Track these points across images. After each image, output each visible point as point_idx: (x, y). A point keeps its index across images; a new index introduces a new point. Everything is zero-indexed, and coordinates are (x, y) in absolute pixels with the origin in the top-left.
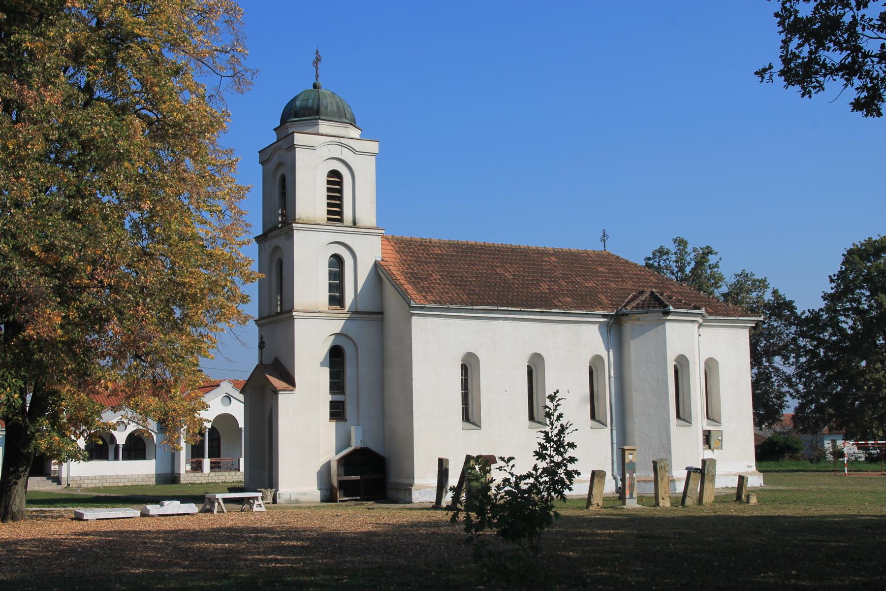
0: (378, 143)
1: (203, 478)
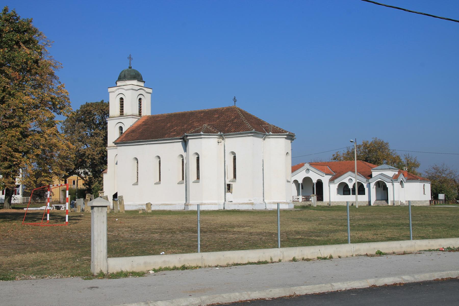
0: (152, 90)
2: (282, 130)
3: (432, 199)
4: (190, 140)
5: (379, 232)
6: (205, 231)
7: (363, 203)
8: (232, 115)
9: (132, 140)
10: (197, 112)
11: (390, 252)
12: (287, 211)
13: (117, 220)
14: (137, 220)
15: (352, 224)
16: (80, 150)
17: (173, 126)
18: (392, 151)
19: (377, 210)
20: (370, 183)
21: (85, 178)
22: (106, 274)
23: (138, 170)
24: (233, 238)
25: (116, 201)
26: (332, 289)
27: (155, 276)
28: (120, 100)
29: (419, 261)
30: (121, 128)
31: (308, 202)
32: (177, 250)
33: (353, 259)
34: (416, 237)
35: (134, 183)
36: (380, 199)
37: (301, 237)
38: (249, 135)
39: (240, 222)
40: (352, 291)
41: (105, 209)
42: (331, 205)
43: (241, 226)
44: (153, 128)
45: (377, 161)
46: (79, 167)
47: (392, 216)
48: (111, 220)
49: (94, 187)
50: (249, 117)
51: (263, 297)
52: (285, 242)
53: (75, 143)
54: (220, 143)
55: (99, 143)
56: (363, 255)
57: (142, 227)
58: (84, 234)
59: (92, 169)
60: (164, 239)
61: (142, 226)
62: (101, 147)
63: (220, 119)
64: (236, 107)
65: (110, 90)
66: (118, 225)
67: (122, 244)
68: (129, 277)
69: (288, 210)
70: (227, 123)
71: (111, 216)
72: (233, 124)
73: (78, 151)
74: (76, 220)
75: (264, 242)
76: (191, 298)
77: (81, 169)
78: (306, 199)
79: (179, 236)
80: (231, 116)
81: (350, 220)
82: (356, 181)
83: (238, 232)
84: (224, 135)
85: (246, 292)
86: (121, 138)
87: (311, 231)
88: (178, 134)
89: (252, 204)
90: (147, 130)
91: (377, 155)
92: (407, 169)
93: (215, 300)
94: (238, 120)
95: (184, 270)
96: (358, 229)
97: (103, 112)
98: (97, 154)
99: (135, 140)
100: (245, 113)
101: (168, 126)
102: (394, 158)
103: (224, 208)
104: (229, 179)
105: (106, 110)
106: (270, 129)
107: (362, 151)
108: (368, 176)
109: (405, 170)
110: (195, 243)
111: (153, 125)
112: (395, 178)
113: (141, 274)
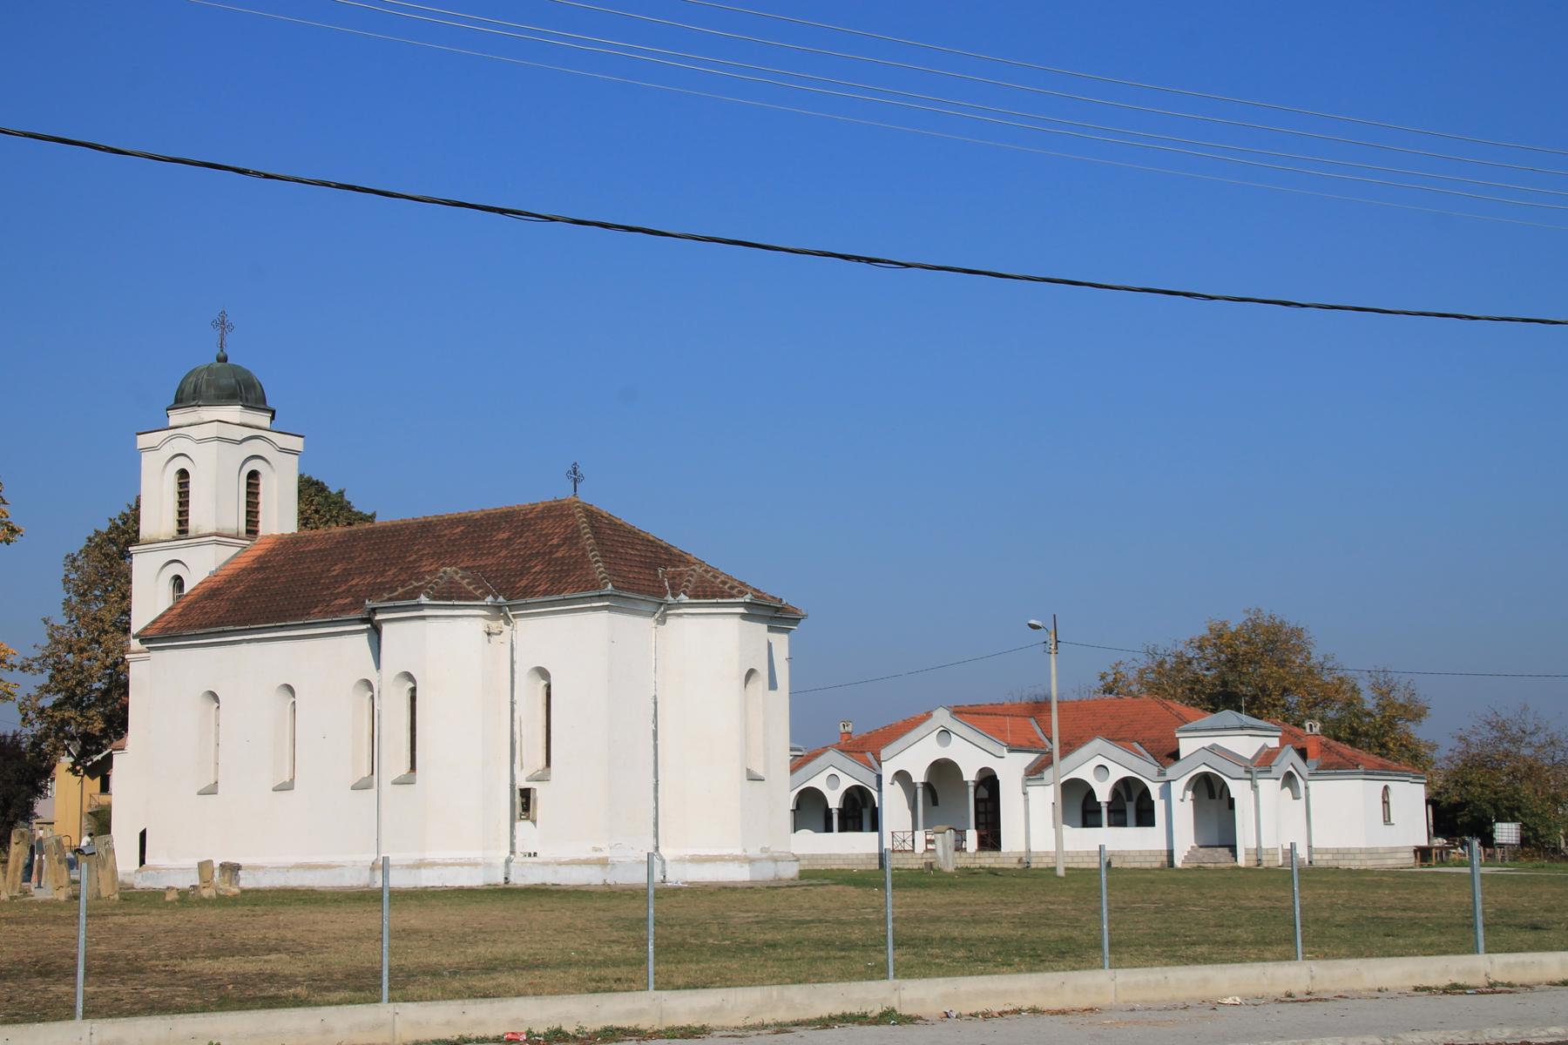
1: (913, 861)
7: (1149, 859)
9: (201, 626)
20: (1169, 781)
28: (180, 478)
30: (178, 582)
35: (205, 788)
36: (1217, 844)
38: (594, 605)
54: (497, 634)
65: (143, 441)
84: (508, 606)
86: (164, 619)
89: (603, 863)
99: (211, 625)
101: (334, 573)
103: (506, 878)
104: (528, 772)
112: (1265, 761)
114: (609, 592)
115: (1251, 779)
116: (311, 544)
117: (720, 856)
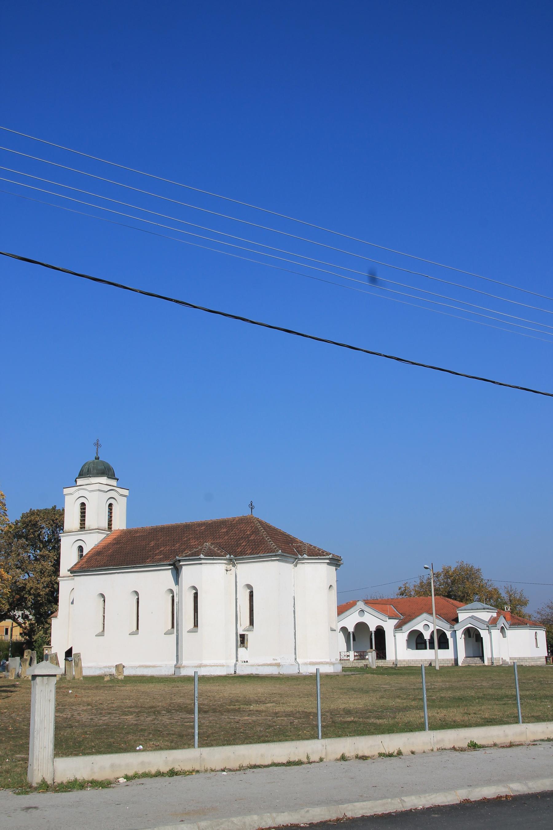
0: (128, 491)
1: (350, 664)
2: (322, 552)
3: (549, 654)
4: (184, 567)
5: (472, 709)
6: (205, 710)
8: (248, 528)
9: (97, 567)
10: (195, 524)
11: (490, 744)
12: (331, 675)
13: (70, 691)
14: (101, 692)
15: (430, 696)
16: (18, 581)
17: (159, 546)
18: (486, 581)
19: (468, 673)
20: (455, 631)
21: (23, 625)
22: (50, 785)
23: (104, 613)
24: (250, 722)
25: (70, 661)
26: (402, 806)
27: (127, 787)
29: (534, 759)
30: (81, 549)
31: (363, 661)
32: (162, 741)
33: (434, 756)
34: (528, 717)
36: (472, 656)
37: (353, 719)
38: (272, 559)
39: (259, 695)
40: (433, 811)
41: (54, 680)
42: (398, 666)
43: (260, 702)
44: (128, 548)
45: (464, 596)
46: (15, 607)
47: (491, 683)
48: (61, 692)
49: (37, 639)
50: (273, 532)
51: (296, 822)
52: (329, 728)
53: (10, 571)
54: (229, 571)
55: (47, 571)
56: (448, 749)
57: (108, 704)
58: (18, 715)
59: (35, 611)
60: (142, 724)
61: (108, 702)
62: (50, 576)
63: (229, 535)
64: (253, 517)
65: (66, 491)
66: (72, 700)
67: (78, 732)
68: (87, 789)
69: (333, 674)
70: (239, 541)
71: (61, 686)
72: (248, 542)
73: (15, 582)
74: (8, 692)
75: (297, 728)
76: (182, 826)
77: (18, 610)
78: (360, 656)
79: (166, 719)
80: (245, 530)
81: (427, 690)
82: (434, 627)
83: (257, 711)
85: (269, 814)
86: (80, 564)
87: (368, 710)
88: (166, 557)
89: (278, 665)
90: (120, 551)
91: (464, 587)
92: (510, 609)
93: (221, 827)
94: (256, 536)
95: (173, 776)
96: (440, 704)
97: (54, 523)
98: (44, 587)
99: (102, 566)
100: (267, 525)
101: (152, 545)
102: (490, 592)
103: (235, 672)
104: (243, 627)
105: (60, 521)
106: (305, 549)
107: (442, 581)
108: (453, 620)
109: (507, 610)
110: (190, 730)
111: (129, 544)
112: (493, 622)
113: (105, 784)
114: (280, 554)
115: (488, 630)
116: (137, 534)
117: (321, 662)
